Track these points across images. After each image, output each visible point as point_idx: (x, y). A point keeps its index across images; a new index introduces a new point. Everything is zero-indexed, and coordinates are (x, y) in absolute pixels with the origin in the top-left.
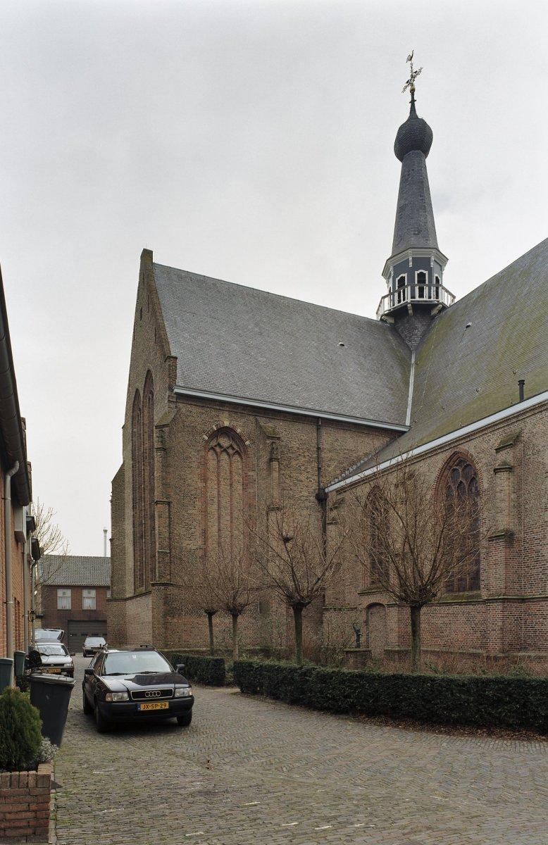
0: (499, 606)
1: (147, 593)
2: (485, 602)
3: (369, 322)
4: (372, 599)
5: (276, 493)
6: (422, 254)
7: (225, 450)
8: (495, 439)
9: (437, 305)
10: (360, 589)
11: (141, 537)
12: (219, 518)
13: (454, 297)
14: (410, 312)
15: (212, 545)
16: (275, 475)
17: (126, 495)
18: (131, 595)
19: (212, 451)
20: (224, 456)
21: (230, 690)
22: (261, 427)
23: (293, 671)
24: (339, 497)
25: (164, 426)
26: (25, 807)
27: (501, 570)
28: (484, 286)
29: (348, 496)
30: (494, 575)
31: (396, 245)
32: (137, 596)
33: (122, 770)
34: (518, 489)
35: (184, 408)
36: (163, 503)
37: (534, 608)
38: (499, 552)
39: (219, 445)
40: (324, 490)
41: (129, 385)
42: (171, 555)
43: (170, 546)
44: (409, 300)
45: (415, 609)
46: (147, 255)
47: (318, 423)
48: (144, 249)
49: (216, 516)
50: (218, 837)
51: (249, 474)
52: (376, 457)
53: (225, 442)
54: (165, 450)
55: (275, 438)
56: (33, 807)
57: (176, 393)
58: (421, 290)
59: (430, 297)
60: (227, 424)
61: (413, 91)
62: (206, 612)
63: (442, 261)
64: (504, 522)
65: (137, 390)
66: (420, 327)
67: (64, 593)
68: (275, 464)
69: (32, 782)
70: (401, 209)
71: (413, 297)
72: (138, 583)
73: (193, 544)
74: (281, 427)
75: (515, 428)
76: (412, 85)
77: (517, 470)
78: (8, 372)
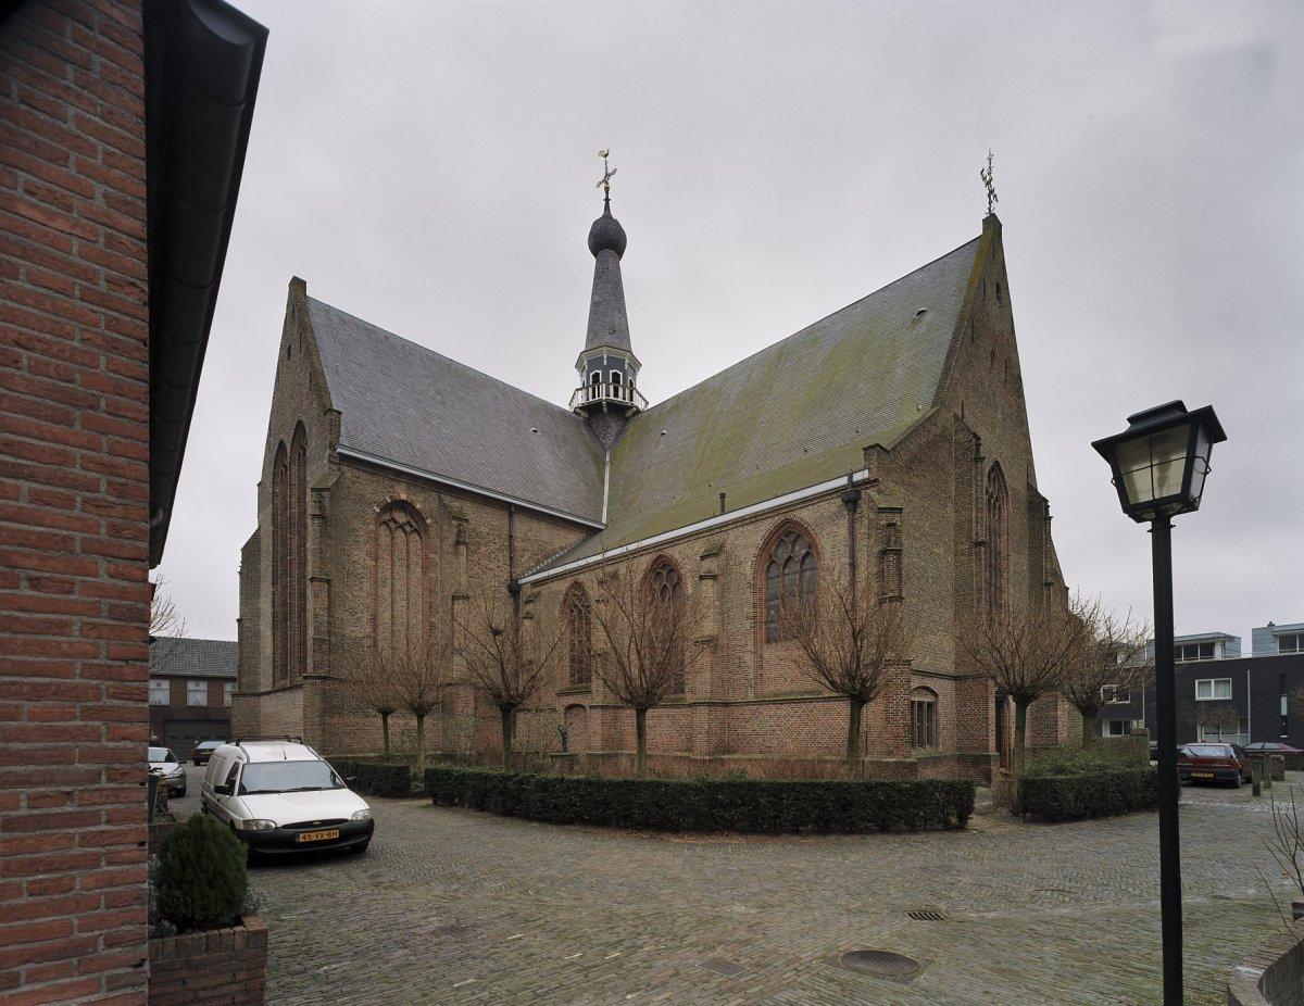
0: (705, 710)
1: (294, 687)
2: (691, 705)
3: (563, 412)
4: (572, 700)
5: (463, 579)
6: (616, 354)
7: (401, 527)
8: (699, 547)
9: (631, 408)
10: (557, 690)
11: (285, 619)
12: (392, 603)
13: (647, 403)
14: (605, 409)
15: (384, 633)
16: (463, 559)
17: (262, 567)
18: (269, 689)
19: (383, 527)
20: (400, 533)
21: (416, 803)
22: (445, 505)
23: (504, 779)
24: (534, 590)
25: (323, 490)
26: (229, 977)
27: (707, 675)
28: (678, 397)
29: (544, 590)
30: (701, 682)
31: (589, 340)
32: (278, 691)
33: (321, 911)
34: (722, 597)
35: (349, 473)
36: (321, 580)
37: (737, 711)
38: (705, 659)
39: (393, 520)
40: (517, 581)
41: (269, 435)
42: (331, 641)
43: (329, 631)
44: (604, 397)
45: (641, 712)
46: (298, 285)
47: (510, 509)
48: (295, 278)
49: (389, 601)
50: (499, 983)
51: (430, 556)
52: (570, 552)
53: (401, 517)
54: (323, 518)
55: (462, 519)
56: (241, 976)
57: (340, 454)
58: (616, 390)
59: (624, 399)
60: (403, 497)
61: (607, 190)
62: (379, 711)
63: (635, 365)
64: (709, 628)
65: (282, 444)
66: (614, 427)
67: (159, 685)
68: (463, 548)
69: (239, 942)
70: (595, 305)
71: (608, 395)
72: (278, 675)
73: (361, 630)
74: (468, 508)
75: (717, 539)
76: (607, 183)
77: (721, 579)
78: (190, 390)
